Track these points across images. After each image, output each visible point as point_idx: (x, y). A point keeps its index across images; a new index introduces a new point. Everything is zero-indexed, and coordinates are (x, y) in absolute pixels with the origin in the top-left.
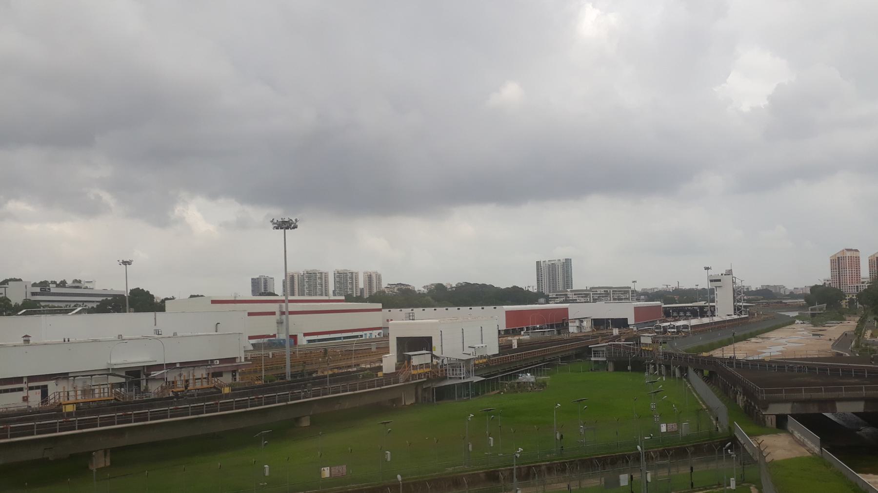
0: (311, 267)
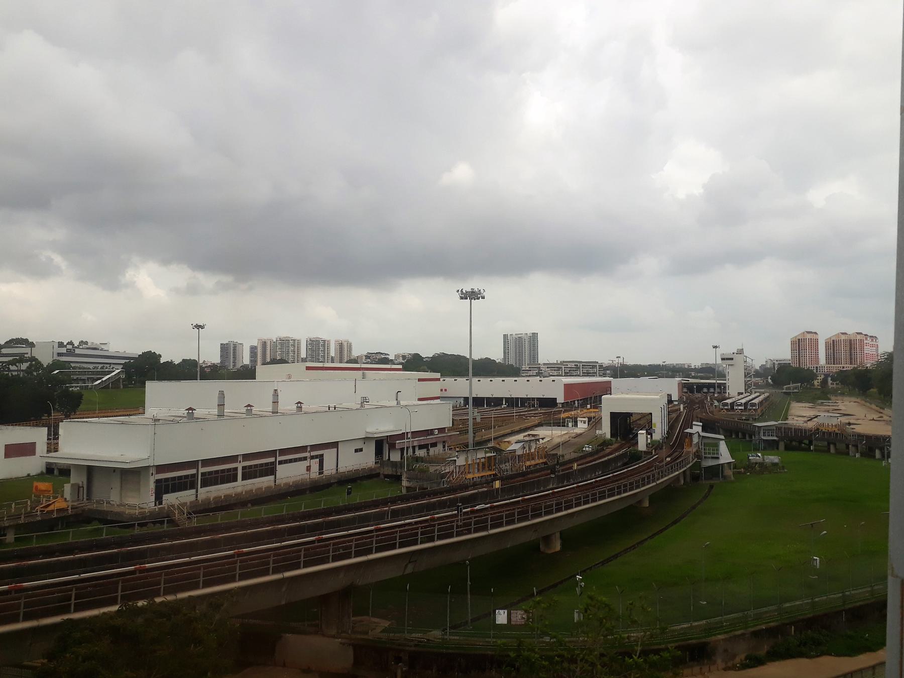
0: (284, 334)
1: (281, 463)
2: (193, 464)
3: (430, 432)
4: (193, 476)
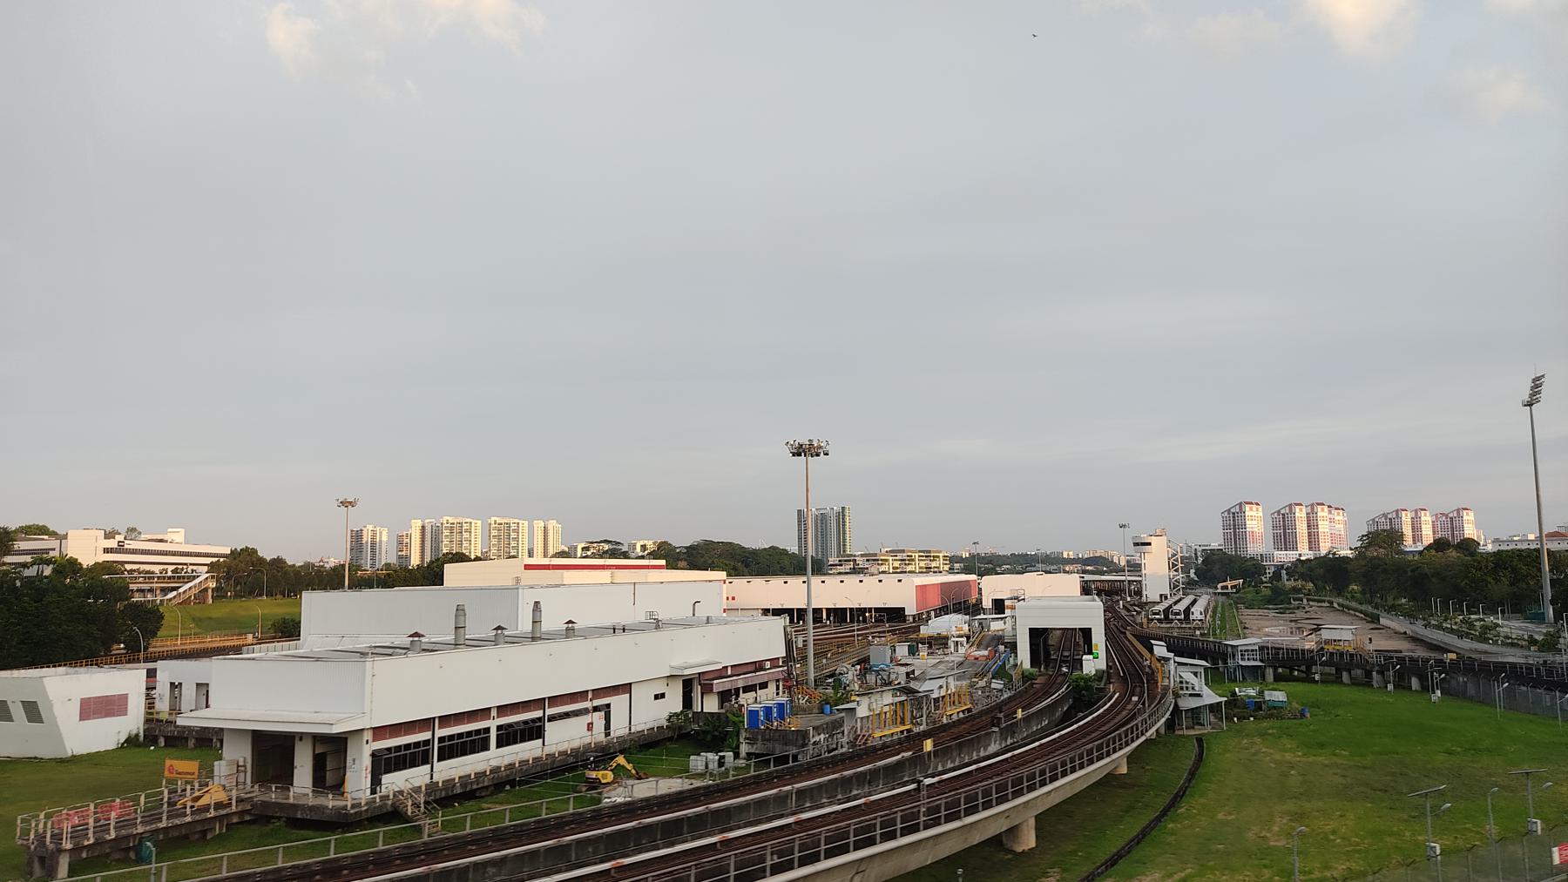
1: (552, 718)
2: (426, 724)
3: (758, 666)
4: (426, 742)
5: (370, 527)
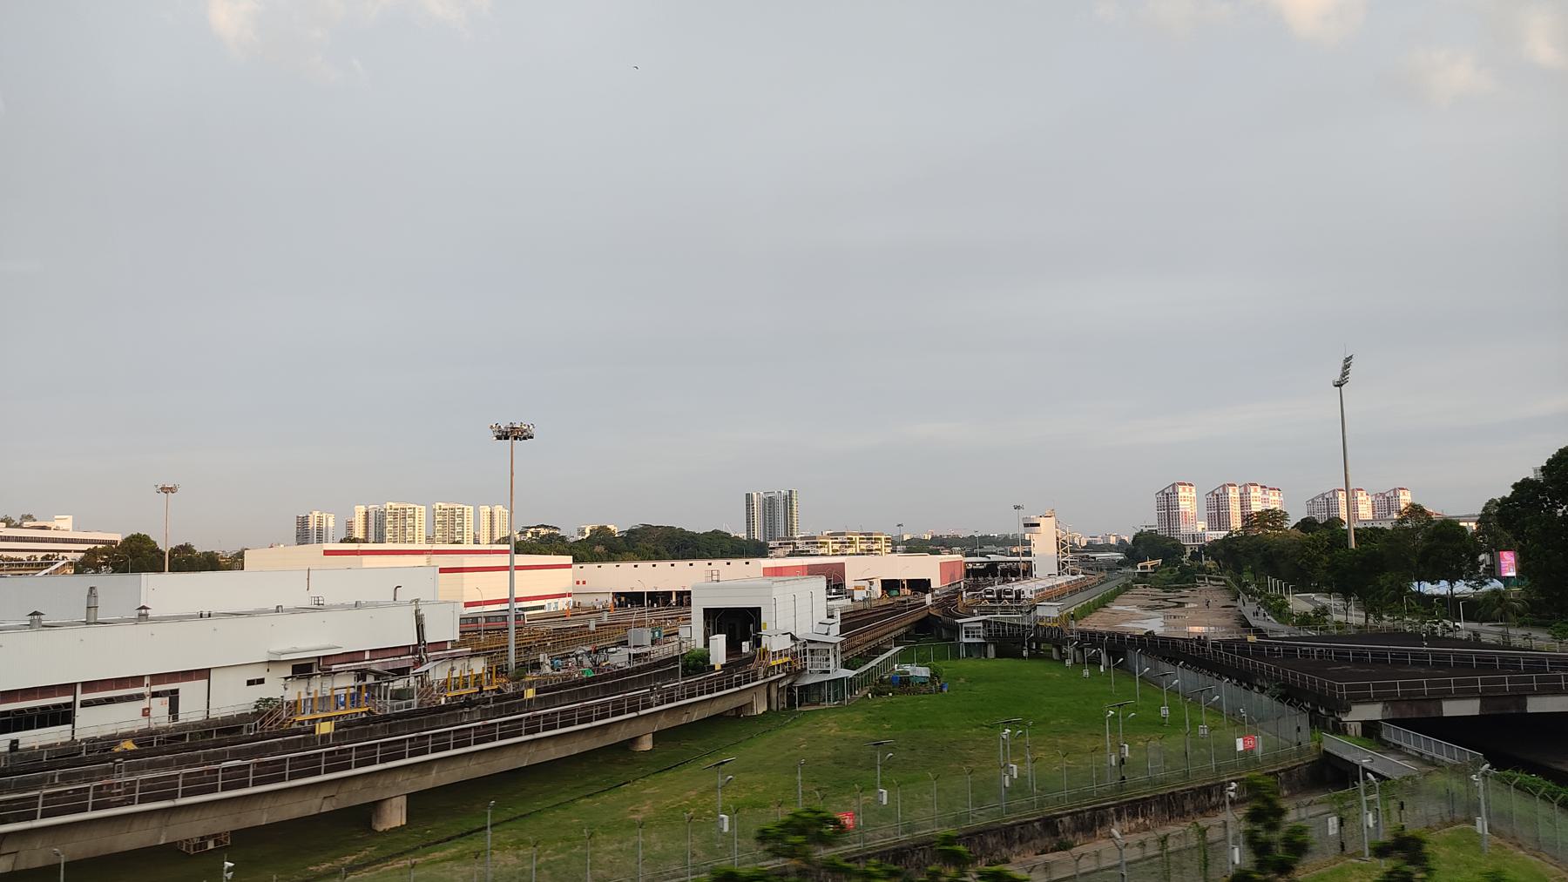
1: (85, 704)
5: (316, 514)
